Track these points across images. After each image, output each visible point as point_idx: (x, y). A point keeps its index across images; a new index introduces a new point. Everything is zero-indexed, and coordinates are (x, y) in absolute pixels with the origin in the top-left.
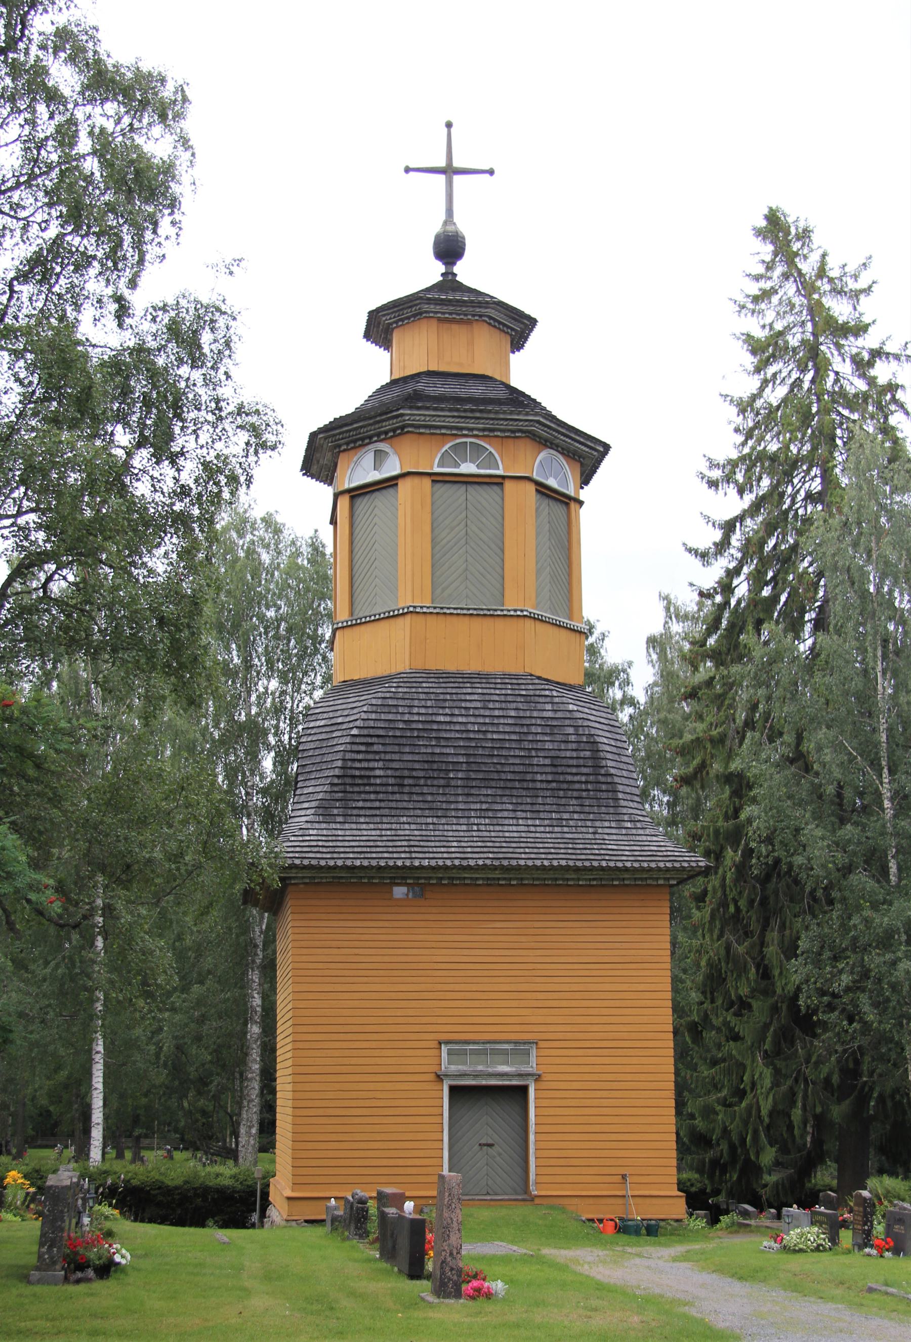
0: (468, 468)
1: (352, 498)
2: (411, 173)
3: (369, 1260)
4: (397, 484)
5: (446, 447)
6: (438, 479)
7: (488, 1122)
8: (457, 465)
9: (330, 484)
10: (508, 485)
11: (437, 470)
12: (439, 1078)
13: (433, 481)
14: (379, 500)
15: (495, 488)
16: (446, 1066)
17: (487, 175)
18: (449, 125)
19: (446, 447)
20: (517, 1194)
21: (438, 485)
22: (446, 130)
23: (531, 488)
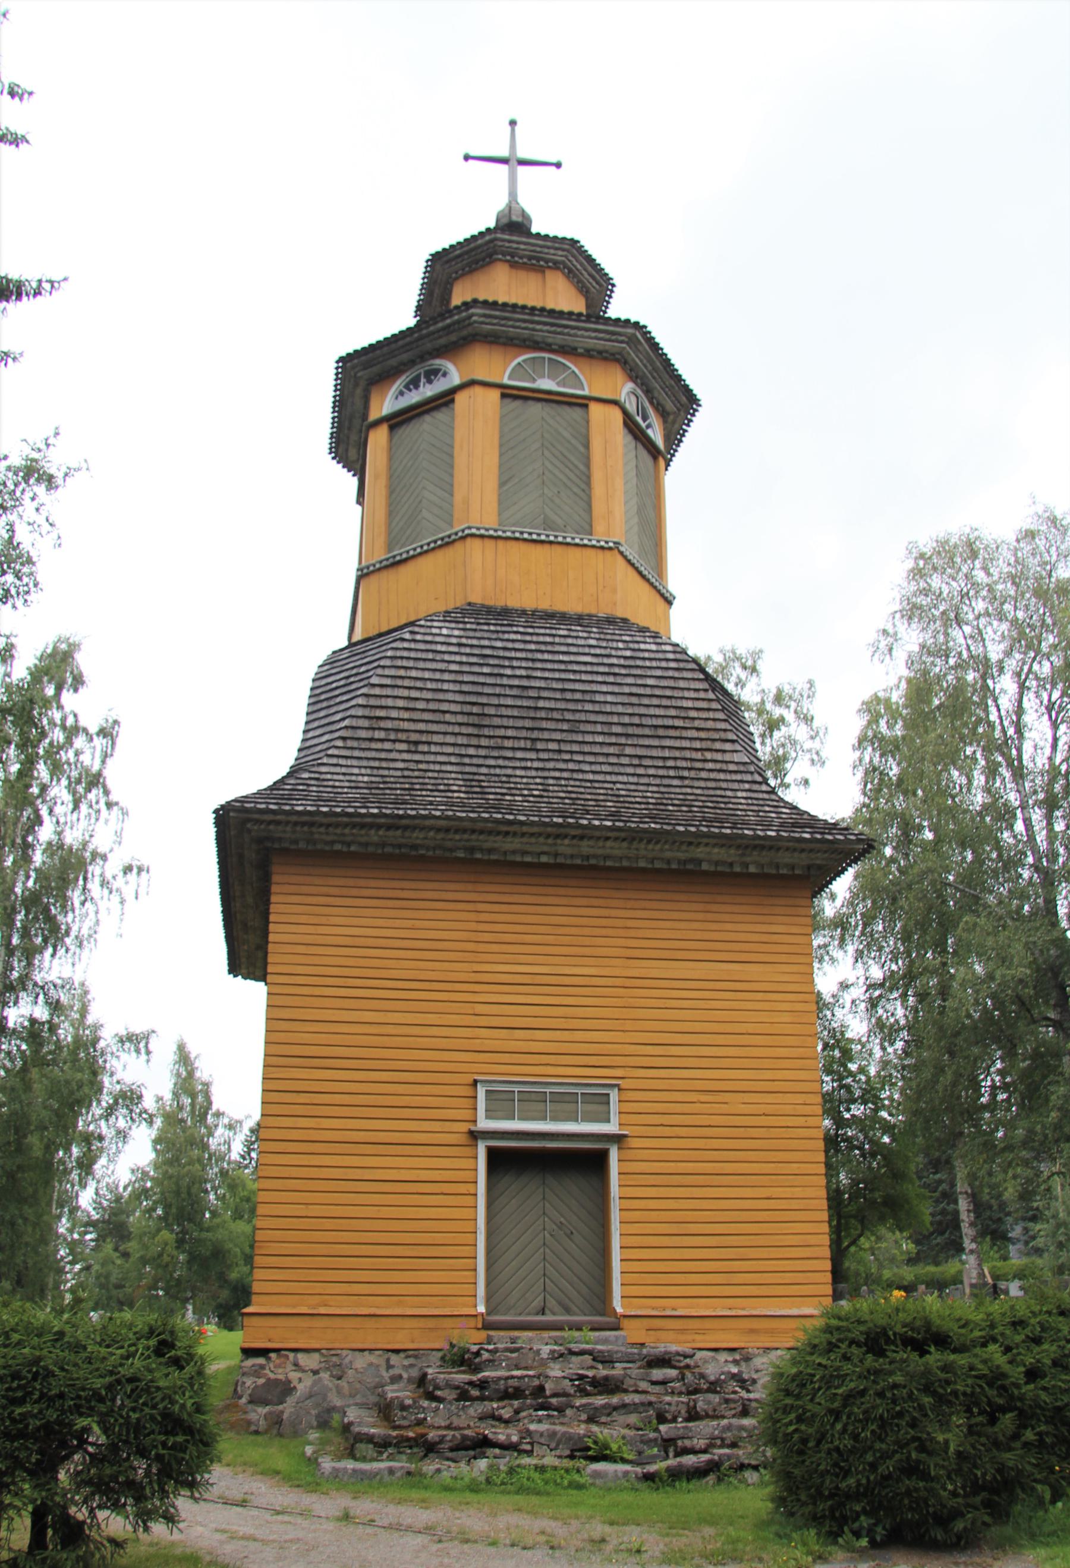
0: (546, 384)
1: (392, 428)
2: (471, 162)
3: (53, 955)
4: (453, 401)
5: (520, 359)
6: (508, 394)
7: (547, 1202)
8: (534, 381)
9: (262, 977)
10: (595, 408)
11: (506, 381)
12: (475, 1136)
13: (504, 396)
14: (427, 424)
15: (578, 410)
16: (484, 1124)
17: (554, 168)
18: (513, 123)
19: (520, 359)
20: (568, 1311)
21: (507, 401)
22: (509, 128)
23: (617, 416)
